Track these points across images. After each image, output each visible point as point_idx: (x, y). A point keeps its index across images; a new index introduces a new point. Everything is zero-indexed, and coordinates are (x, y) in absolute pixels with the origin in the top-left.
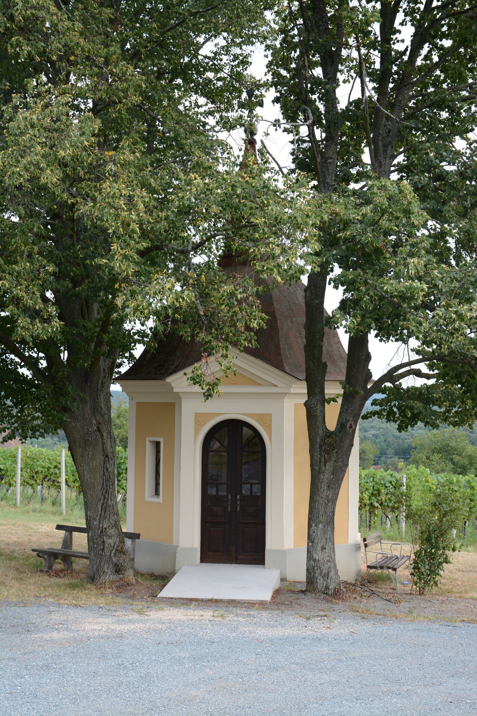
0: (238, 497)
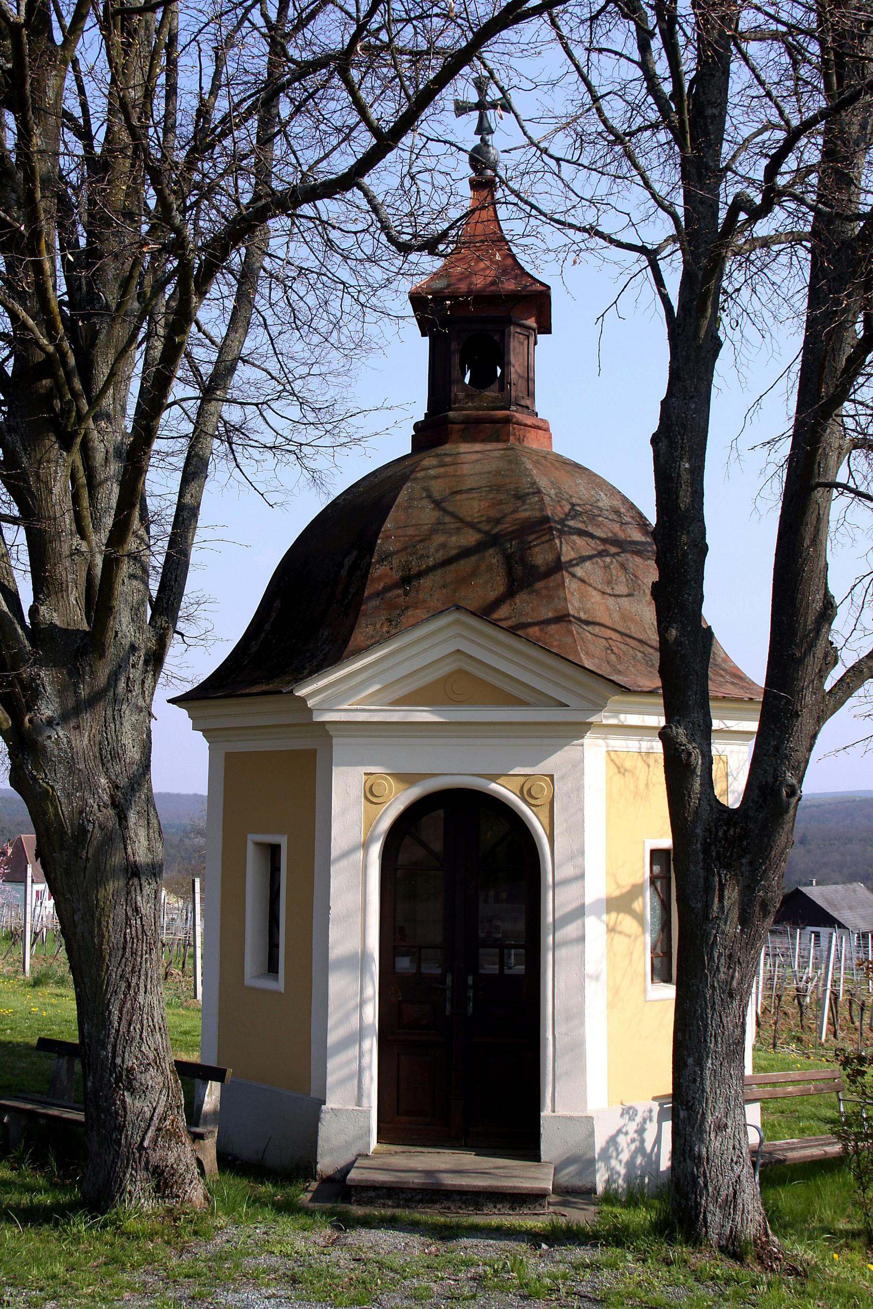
0: (470, 980)
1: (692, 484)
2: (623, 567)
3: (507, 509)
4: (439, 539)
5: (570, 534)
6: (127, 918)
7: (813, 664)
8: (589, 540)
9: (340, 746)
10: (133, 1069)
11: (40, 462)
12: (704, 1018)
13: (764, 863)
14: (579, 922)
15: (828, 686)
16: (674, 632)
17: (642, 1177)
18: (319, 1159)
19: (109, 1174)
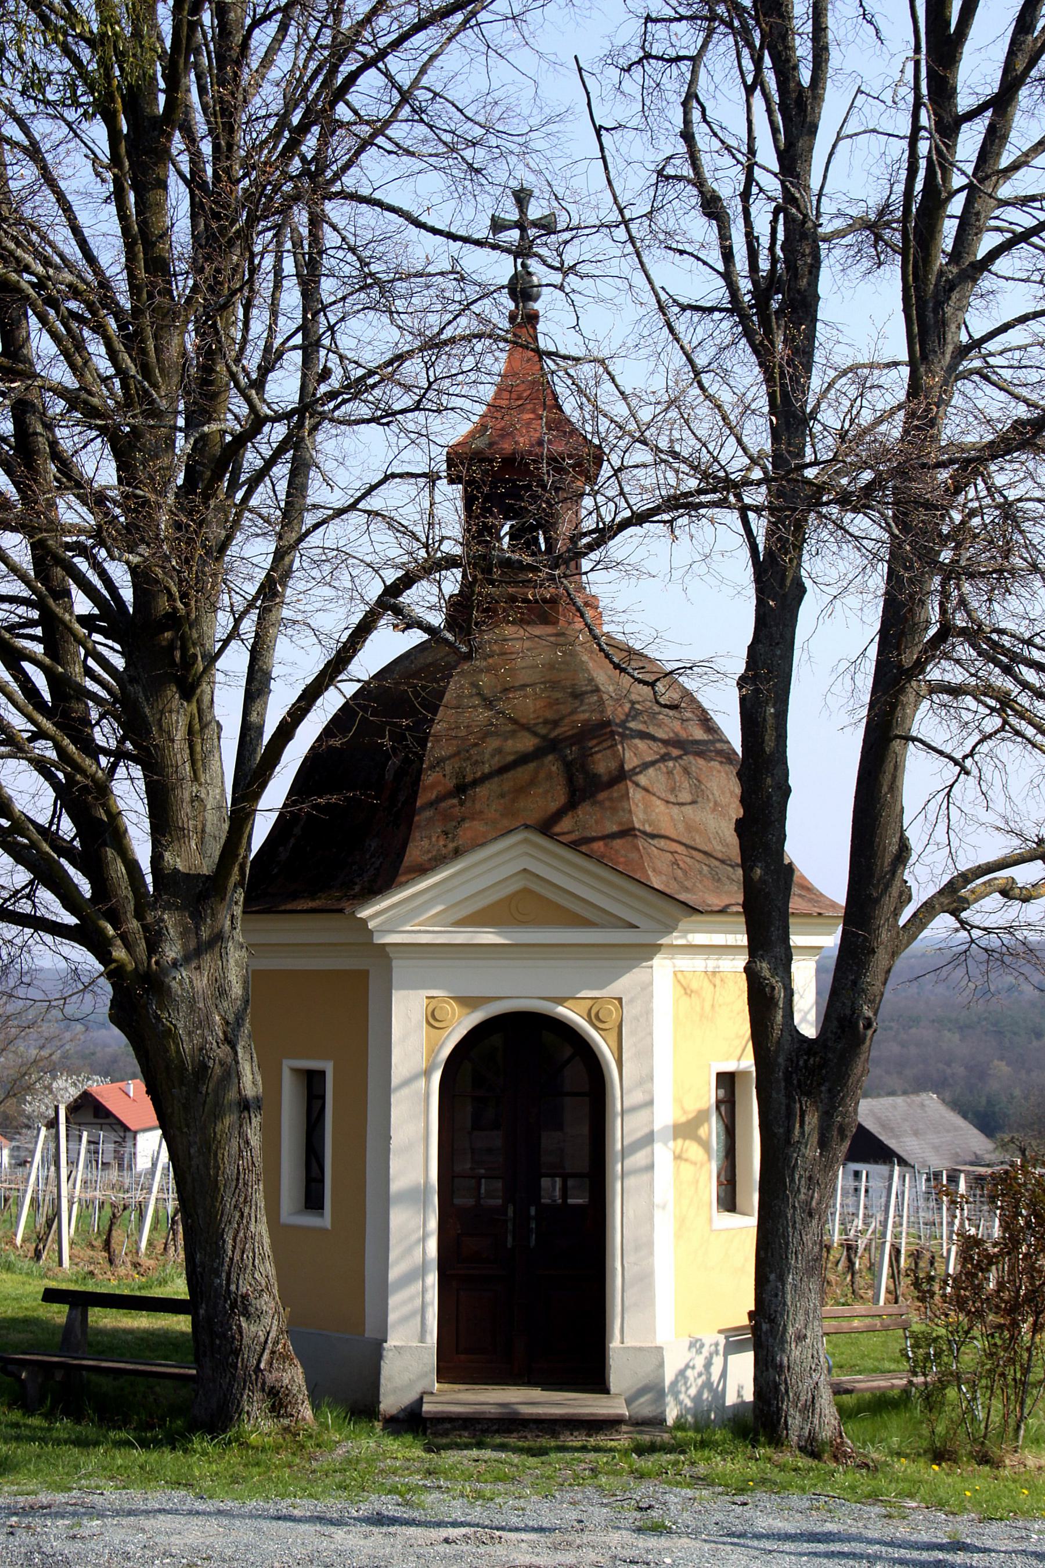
0: (533, 1211)
1: (776, 729)
2: (686, 771)
3: (564, 709)
4: (493, 743)
5: (633, 737)
6: (240, 1151)
7: (888, 903)
8: (651, 743)
9: (399, 968)
10: (247, 1295)
11: (162, 712)
12: (785, 1236)
13: (842, 1090)
14: (648, 1149)
15: (902, 921)
16: (759, 871)
17: (709, 1411)
18: (382, 1398)
19: (225, 1395)
